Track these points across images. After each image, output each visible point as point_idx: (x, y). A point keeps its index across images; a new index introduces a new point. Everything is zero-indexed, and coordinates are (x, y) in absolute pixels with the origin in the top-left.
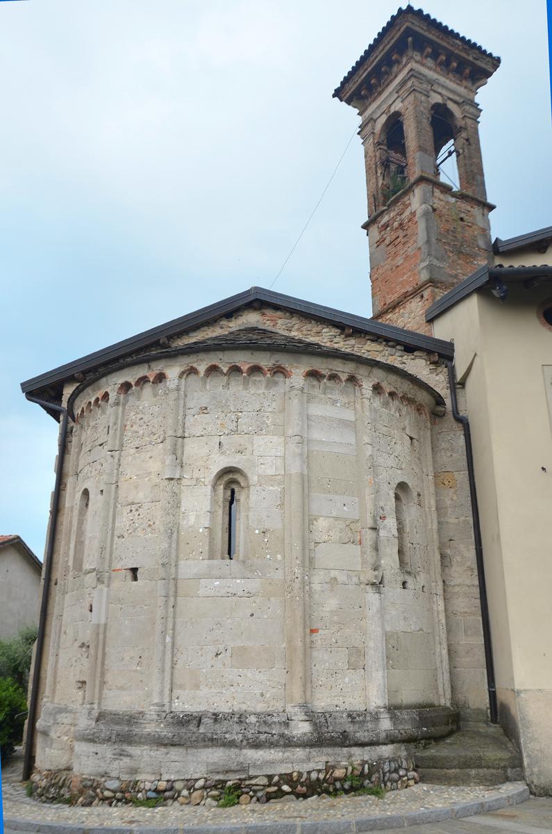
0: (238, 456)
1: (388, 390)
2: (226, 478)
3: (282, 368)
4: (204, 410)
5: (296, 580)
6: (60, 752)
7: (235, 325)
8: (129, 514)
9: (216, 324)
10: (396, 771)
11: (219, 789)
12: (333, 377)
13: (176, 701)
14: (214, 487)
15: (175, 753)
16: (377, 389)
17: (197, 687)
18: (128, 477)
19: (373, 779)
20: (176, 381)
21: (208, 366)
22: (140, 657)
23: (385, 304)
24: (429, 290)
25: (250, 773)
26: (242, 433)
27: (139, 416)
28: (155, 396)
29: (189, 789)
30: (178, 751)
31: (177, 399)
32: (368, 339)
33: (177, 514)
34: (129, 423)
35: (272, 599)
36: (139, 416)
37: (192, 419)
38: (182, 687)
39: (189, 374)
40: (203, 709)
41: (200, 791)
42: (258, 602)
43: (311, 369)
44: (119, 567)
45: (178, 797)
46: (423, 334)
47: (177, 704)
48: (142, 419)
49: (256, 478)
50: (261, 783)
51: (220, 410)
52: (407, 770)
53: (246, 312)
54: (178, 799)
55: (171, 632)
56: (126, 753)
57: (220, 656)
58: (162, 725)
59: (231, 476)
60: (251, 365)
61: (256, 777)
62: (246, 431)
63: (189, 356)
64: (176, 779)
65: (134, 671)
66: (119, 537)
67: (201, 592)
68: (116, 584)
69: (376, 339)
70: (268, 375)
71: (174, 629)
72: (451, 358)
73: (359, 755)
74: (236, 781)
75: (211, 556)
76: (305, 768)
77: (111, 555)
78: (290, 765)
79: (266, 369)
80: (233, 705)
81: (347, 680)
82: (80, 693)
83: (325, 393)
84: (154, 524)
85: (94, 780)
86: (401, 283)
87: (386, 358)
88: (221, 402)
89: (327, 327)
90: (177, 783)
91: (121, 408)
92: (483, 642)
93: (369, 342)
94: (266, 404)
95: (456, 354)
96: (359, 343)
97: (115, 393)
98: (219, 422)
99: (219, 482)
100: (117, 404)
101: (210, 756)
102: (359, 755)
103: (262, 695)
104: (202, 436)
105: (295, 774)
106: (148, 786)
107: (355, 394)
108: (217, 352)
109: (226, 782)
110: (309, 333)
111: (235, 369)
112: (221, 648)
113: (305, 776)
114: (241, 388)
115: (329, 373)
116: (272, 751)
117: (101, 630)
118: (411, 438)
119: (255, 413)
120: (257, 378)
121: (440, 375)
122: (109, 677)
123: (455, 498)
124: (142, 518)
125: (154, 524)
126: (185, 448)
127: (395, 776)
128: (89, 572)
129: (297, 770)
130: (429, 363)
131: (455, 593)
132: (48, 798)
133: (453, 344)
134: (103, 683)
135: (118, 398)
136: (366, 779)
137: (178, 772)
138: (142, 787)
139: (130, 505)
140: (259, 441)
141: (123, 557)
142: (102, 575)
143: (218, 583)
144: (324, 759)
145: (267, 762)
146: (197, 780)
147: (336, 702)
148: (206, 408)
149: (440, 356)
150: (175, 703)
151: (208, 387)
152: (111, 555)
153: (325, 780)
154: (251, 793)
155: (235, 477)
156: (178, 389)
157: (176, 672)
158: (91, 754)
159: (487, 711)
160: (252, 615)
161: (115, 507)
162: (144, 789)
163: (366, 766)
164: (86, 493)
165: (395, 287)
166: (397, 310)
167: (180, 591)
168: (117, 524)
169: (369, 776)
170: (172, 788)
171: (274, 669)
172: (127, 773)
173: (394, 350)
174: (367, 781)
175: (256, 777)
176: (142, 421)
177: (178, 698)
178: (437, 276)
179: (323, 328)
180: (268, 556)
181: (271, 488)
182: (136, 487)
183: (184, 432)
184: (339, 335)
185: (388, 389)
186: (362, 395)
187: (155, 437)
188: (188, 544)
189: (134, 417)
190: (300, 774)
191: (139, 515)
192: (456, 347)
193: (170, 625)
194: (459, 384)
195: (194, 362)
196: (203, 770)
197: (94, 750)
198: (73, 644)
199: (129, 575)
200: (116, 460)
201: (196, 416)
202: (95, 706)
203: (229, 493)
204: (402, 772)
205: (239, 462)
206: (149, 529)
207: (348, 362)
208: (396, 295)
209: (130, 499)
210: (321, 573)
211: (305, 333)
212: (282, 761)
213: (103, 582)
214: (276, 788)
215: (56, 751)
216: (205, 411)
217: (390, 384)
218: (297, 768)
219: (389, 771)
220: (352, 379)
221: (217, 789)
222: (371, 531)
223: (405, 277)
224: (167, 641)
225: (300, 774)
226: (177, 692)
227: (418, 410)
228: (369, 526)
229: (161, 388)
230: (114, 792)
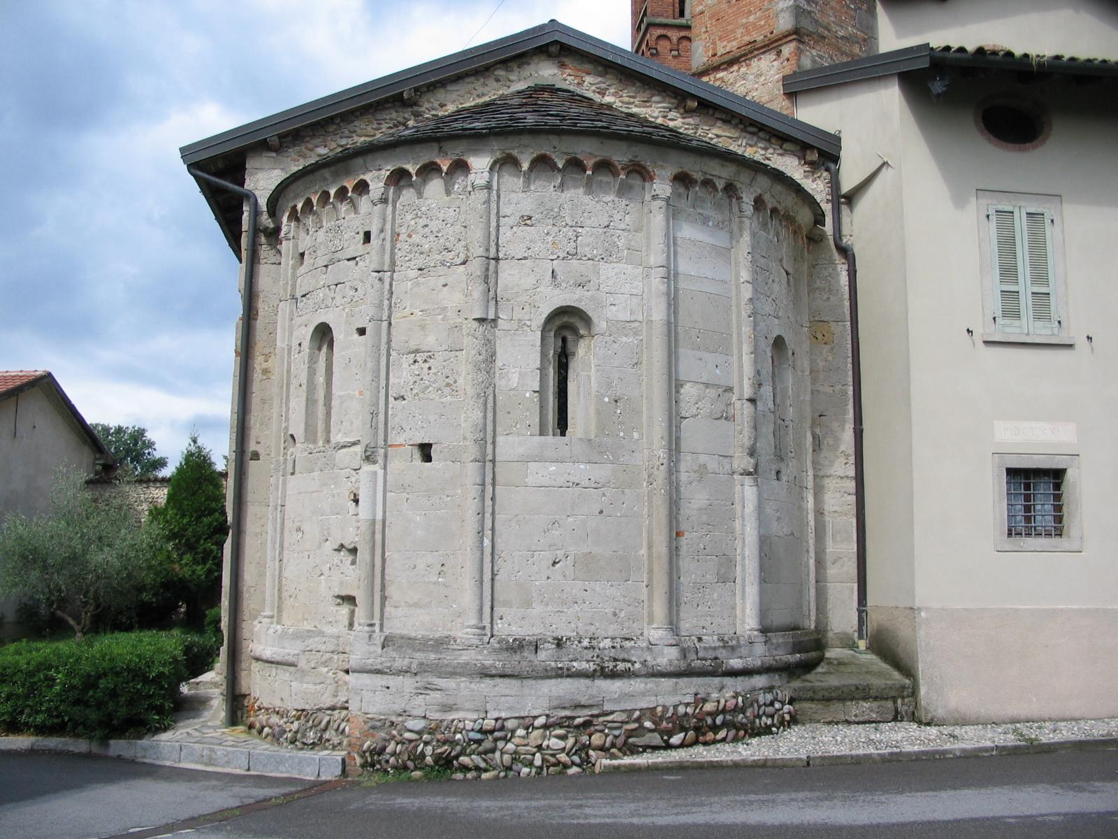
0: (579, 291)
1: (770, 206)
2: (558, 322)
3: (640, 166)
4: (527, 220)
5: (662, 468)
6: (318, 687)
7: (519, 82)
8: (412, 367)
9: (487, 74)
10: (772, 704)
11: (564, 727)
12: (708, 183)
13: (499, 621)
14: (544, 330)
15: (504, 686)
16: (759, 203)
17: (528, 604)
18: (407, 312)
19: (748, 714)
20: (486, 175)
21: (535, 155)
22: (443, 565)
23: (714, 55)
24: (793, 45)
25: (605, 708)
26: (584, 258)
27: (422, 222)
28: (448, 192)
29: (527, 728)
30: (510, 684)
31: (488, 201)
32: (718, 119)
33: (492, 371)
34: (403, 230)
35: (626, 491)
36: (422, 222)
37: (509, 234)
38: (507, 604)
39: (503, 164)
40: (537, 632)
41: (541, 730)
42: (608, 494)
43: (680, 170)
44: (400, 440)
45: (511, 737)
46: (779, 110)
47: (500, 626)
48: (427, 226)
49: (604, 325)
50: (619, 720)
51: (551, 221)
52: (783, 703)
53: (536, 60)
54: (513, 740)
55: (490, 532)
56: (435, 687)
57: (557, 566)
58: (485, 652)
59: (565, 319)
60: (598, 158)
61: (612, 713)
62: (589, 256)
63: (506, 138)
64: (508, 716)
65: (434, 583)
66: (396, 399)
67: (530, 480)
68: (395, 465)
69: (729, 118)
70: (622, 176)
71: (493, 529)
72: (836, 159)
73: (734, 686)
74: (587, 718)
75: (542, 432)
76: (670, 701)
77: (386, 424)
78: (654, 698)
79: (620, 167)
80: (577, 627)
81: (716, 596)
82: (344, 612)
83: (694, 207)
84: (455, 382)
85: (386, 719)
86: (745, 26)
87: (743, 149)
88: (552, 210)
89: (658, 95)
90: (509, 721)
91: (390, 208)
92: (855, 550)
93: (719, 124)
94: (617, 217)
95: (843, 154)
96: (706, 123)
97: (382, 184)
98: (550, 238)
99: (549, 327)
100: (384, 200)
101: (554, 688)
102: (732, 685)
103: (615, 614)
104: (525, 258)
105: (660, 709)
106: (469, 725)
107: (731, 209)
108: (551, 137)
109: (573, 718)
110: (632, 100)
111: (575, 164)
112: (560, 554)
113: (671, 710)
114: (581, 191)
115: (702, 178)
116: (632, 682)
117: (378, 527)
118: (787, 274)
119: (601, 231)
120: (606, 178)
121: (818, 181)
122: (391, 590)
123: (830, 358)
124: (435, 374)
125: (455, 382)
126: (500, 275)
127: (770, 710)
128: (345, 447)
129: (662, 704)
130: (803, 162)
131: (208, 453)
132: (304, 744)
133: (840, 139)
134: (384, 599)
135: (385, 193)
136: (739, 714)
137: (510, 708)
138: (462, 727)
139: (412, 353)
140: (609, 273)
141: (406, 427)
142: (373, 452)
143: (554, 468)
144: (693, 690)
145: (626, 694)
146: (535, 717)
147: (702, 623)
148: (530, 218)
149: (822, 153)
150: (497, 624)
151: (532, 188)
152: (386, 424)
153: (694, 716)
154: (606, 731)
155: (572, 320)
156: (488, 187)
157: (497, 584)
158: (380, 688)
159: (853, 635)
160: (601, 512)
161: (389, 355)
162: (464, 728)
163: (740, 699)
164: (323, 334)
165: (733, 31)
166: (735, 68)
167: (498, 478)
168: (392, 380)
169: (743, 710)
170: (502, 728)
171: (630, 582)
172: (437, 711)
173: (755, 139)
174: (741, 716)
175: (612, 713)
176: (427, 229)
177: (501, 619)
178: (807, 24)
179: (653, 95)
180: (622, 434)
181: (624, 339)
182: (423, 327)
183: (497, 250)
184: (676, 108)
185: (770, 203)
186: (741, 212)
187: (451, 255)
188: (509, 413)
189: (413, 222)
190: (665, 708)
191: (430, 368)
192: (844, 144)
193: (488, 524)
194: (844, 196)
195: (513, 149)
196: (546, 705)
197: (385, 683)
198: (319, 547)
199: (417, 454)
200: (387, 286)
201: (515, 229)
202: (377, 628)
203: (560, 343)
204: (777, 705)
205: (580, 300)
206: (447, 390)
207: (727, 164)
208: (734, 43)
209: (413, 346)
210: (689, 458)
211: (626, 99)
212: (643, 694)
213: (375, 462)
214: (636, 725)
215: (310, 686)
216: (528, 222)
217: (773, 196)
218: (661, 701)
219: (765, 704)
220: (730, 189)
221: (561, 727)
222: (748, 404)
223: (752, 18)
224: (485, 545)
225: (665, 708)
226: (499, 610)
227: (795, 232)
228: (746, 396)
229: (459, 183)
230: (419, 733)
